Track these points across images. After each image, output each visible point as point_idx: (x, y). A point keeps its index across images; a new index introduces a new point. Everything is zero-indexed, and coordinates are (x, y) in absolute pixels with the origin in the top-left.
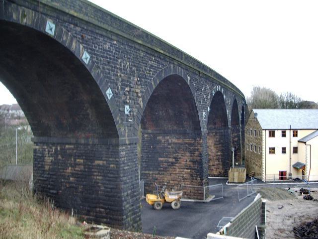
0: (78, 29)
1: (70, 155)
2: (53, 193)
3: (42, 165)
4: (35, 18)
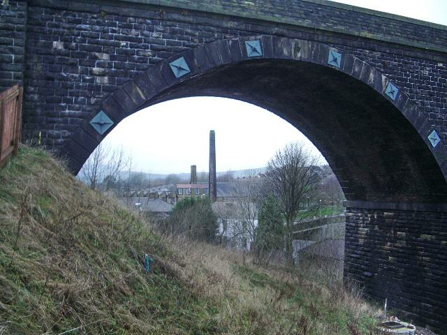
0: (378, 54)
1: (390, 226)
2: (366, 276)
3: (356, 237)
4: (312, 50)
